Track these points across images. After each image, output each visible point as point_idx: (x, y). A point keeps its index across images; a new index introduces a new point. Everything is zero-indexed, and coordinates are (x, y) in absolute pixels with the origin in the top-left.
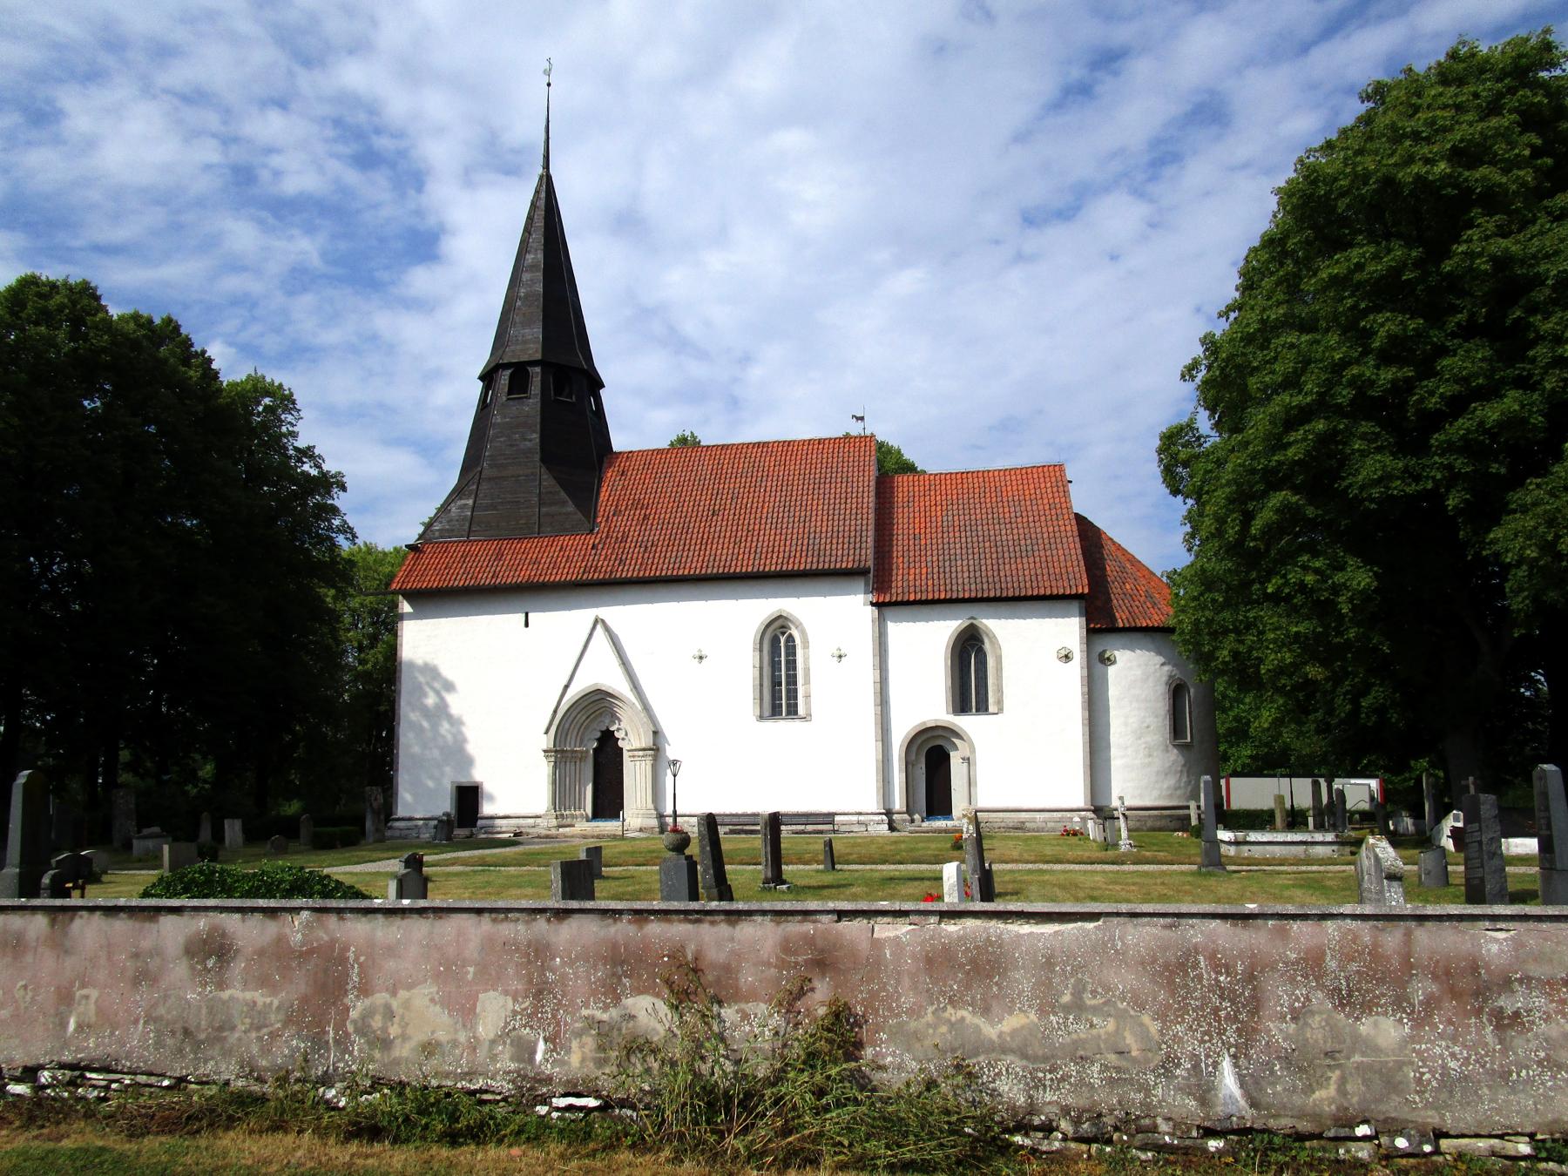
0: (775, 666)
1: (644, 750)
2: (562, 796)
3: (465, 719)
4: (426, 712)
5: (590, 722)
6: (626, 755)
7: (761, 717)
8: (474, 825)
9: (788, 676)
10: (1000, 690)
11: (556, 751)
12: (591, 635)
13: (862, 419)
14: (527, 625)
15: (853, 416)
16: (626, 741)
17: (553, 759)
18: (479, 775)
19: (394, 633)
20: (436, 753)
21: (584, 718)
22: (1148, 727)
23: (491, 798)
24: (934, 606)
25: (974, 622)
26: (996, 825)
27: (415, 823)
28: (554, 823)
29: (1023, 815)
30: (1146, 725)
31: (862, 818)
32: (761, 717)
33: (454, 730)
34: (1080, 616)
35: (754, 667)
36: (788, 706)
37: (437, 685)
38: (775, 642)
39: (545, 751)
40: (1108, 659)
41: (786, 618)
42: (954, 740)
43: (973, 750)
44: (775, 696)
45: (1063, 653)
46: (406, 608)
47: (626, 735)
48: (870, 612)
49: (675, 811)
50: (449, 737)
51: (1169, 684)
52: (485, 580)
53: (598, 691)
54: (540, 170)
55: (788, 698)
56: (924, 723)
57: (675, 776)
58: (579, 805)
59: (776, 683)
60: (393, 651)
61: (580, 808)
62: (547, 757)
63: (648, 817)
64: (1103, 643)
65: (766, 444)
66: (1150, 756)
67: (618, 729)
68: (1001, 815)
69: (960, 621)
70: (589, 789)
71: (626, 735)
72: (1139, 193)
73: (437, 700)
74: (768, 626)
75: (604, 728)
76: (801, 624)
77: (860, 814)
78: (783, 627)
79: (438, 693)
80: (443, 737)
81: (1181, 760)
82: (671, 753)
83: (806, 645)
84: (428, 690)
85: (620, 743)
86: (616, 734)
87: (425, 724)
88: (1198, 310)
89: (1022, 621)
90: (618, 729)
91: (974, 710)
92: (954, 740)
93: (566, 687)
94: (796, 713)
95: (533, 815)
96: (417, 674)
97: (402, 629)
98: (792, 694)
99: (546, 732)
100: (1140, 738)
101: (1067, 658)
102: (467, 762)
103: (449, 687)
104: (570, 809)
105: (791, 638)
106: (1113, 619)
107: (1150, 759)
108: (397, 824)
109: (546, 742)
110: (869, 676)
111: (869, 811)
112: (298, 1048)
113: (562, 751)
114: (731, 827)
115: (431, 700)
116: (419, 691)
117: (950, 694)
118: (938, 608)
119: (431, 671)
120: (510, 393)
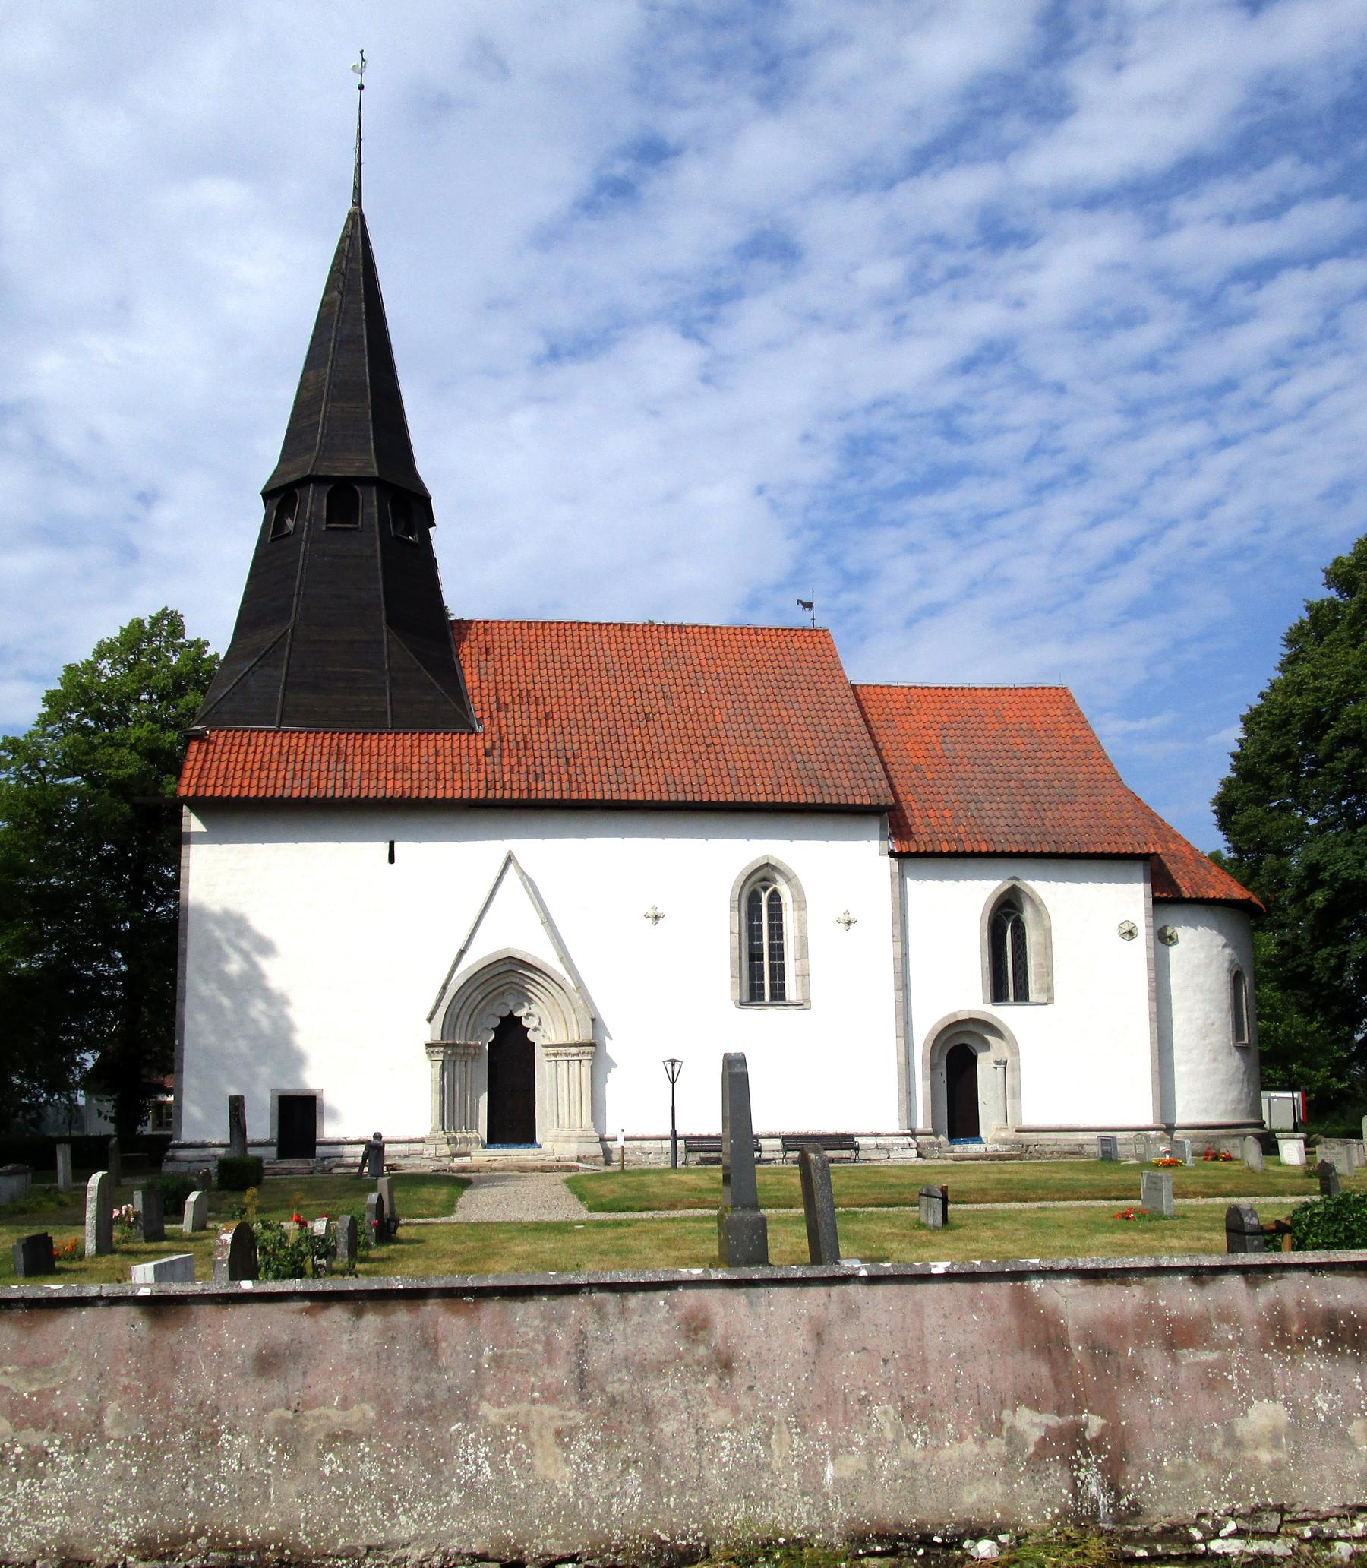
0: (754, 932)
1: (576, 1045)
2: (451, 1113)
3: (292, 996)
4: (226, 984)
5: (486, 1004)
6: (539, 1054)
7: (741, 1004)
8: (313, 1155)
9: (771, 947)
10: (1048, 972)
11: (446, 1046)
12: (500, 878)
13: (810, 606)
14: (392, 860)
15: (799, 602)
16: (539, 1034)
17: (441, 1056)
18: (311, 1080)
19: (175, 860)
20: (243, 1046)
21: (480, 997)
22: (1213, 1024)
23: (334, 1115)
24: (939, 860)
25: (1017, 883)
26: (1048, 1149)
27: (212, 1151)
28: (446, 1149)
29: (1080, 1136)
30: (1209, 1021)
31: (881, 1141)
32: (741, 1004)
33: (274, 1013)
34: (1145, 881)
35: (731, 933)
36: (772, 987)
37: (244, 944)
38: (754, 899)
39: (428, 1045)
40: (1171, 937)
41: (774, 868)
42: (988, 1037)
43: (1015, 1050)
44: (755, 973)
45: (1127, 928)
46: (193, 824)
47: (540, 1023)
48: (887, 864)
49: (674, 1132)
50: (265, 1024)
51: (1230, 971)
52: (333, 790)
53: (511, 960)
54: (348, 206)
55: (772, 977)
56: (955, 1014)
57: (673, 1083)
58: (473, 1127)
59: (755, 956)
60: (173, 887)
61: (472, 1129)
62: (430, 1054)
63: (588, 1140)
64: (1171, 914)
65: (681, 628)
66: (1215, 1060)
67: (528, 1015)
68: (1053, 1135)
69: (999, 882)
70: (484, 1100)
71: (540, 1023)
72: (689, 331)
73: (246, 967)
74: (749, 877)
75: (505, 1014)
76: (795, 876)
77: (878, 1135)
78: (764, 879)
79: (246, 956)
80: (254, 1021)
81: (1242, 1065)
82: (611, 1048)
83: (801, 904)
84: (228, 950)
85: (531, 1036)
86: (525, 1023)
87: (226, 1002)
88: (760, 490)
89: (1075, 885)
90: (528, 1015)
91: (1011, 998)
92: (988, 1037)
93: (462, 952)
94: (782, 997)
95: (407, 1138)
96: (211, 926)
97: (188, 857)
98: (778, 972)
99: (430, 1020)
100: (1204, 1038)
101: (1131, 934)
102: (295, 1060)
103: (266, 947)
104: (460, 1129)
105: (775, 896)
106: (1178, 888)
107: (1215, 1065)
108: (182, 1153)
109: (430, 1032)
110: (887, 950)
111: (891, 1132)
112: (326, 1501)
113: (454, 1045)
114: (702, 1154)
115: (234, 966)
116: (215, 950)
117: (987, 977)
118: (973, 864)
119: (236, 924)
120: (329, 520)
